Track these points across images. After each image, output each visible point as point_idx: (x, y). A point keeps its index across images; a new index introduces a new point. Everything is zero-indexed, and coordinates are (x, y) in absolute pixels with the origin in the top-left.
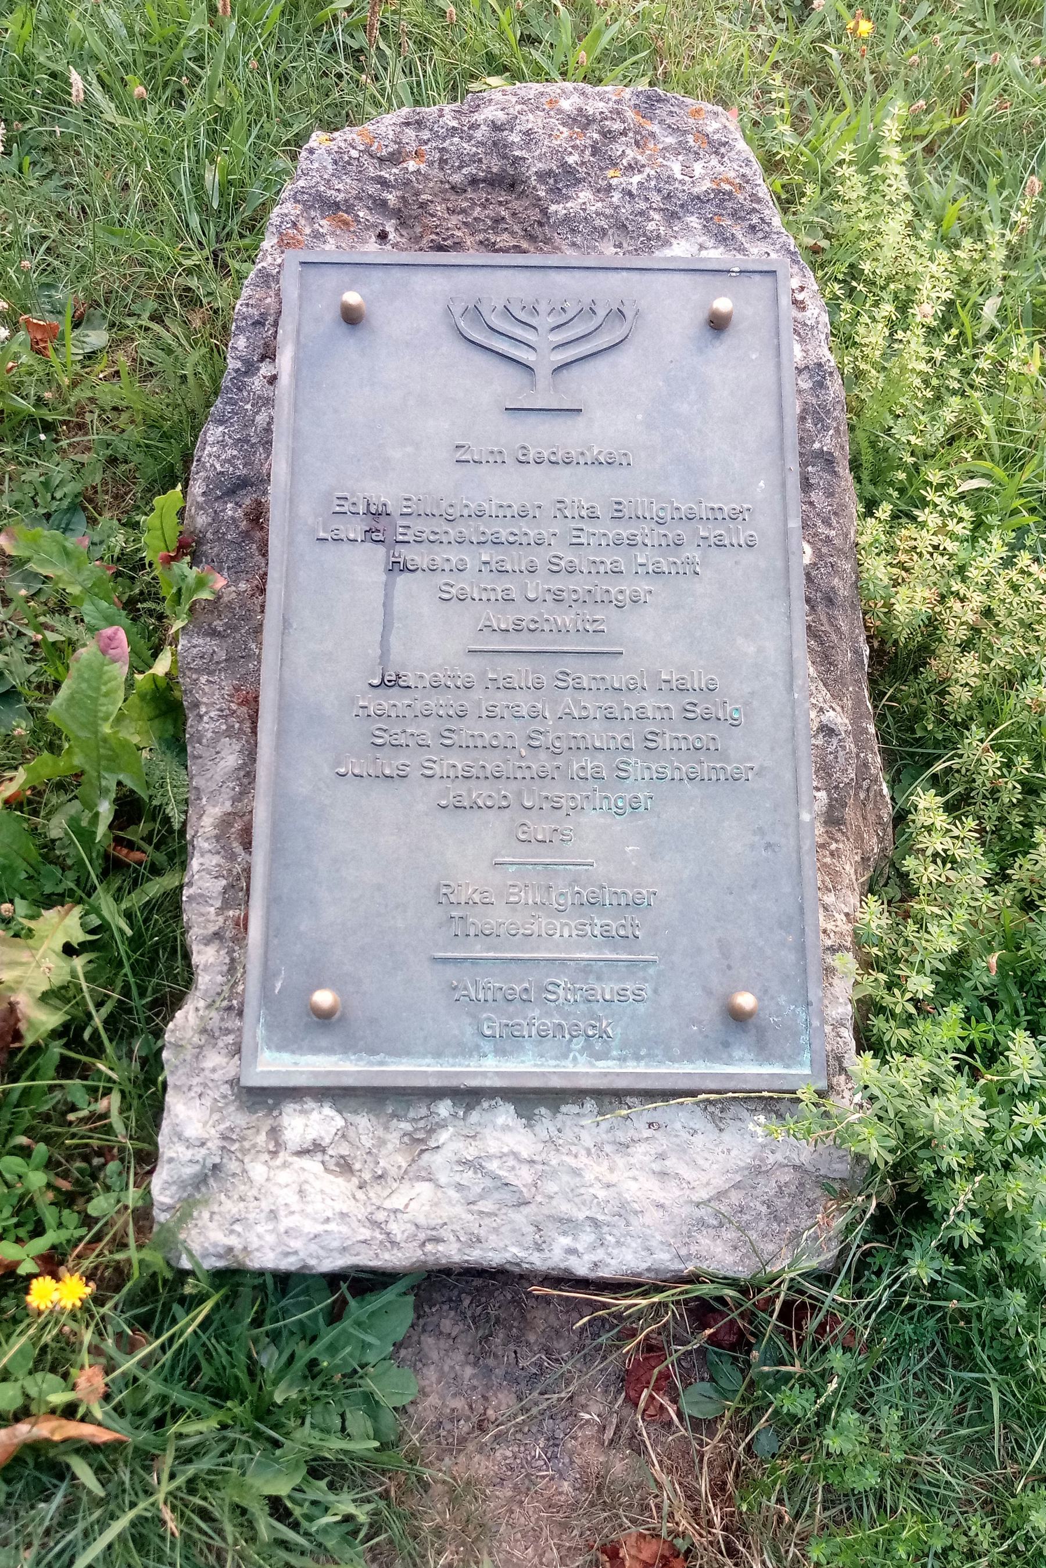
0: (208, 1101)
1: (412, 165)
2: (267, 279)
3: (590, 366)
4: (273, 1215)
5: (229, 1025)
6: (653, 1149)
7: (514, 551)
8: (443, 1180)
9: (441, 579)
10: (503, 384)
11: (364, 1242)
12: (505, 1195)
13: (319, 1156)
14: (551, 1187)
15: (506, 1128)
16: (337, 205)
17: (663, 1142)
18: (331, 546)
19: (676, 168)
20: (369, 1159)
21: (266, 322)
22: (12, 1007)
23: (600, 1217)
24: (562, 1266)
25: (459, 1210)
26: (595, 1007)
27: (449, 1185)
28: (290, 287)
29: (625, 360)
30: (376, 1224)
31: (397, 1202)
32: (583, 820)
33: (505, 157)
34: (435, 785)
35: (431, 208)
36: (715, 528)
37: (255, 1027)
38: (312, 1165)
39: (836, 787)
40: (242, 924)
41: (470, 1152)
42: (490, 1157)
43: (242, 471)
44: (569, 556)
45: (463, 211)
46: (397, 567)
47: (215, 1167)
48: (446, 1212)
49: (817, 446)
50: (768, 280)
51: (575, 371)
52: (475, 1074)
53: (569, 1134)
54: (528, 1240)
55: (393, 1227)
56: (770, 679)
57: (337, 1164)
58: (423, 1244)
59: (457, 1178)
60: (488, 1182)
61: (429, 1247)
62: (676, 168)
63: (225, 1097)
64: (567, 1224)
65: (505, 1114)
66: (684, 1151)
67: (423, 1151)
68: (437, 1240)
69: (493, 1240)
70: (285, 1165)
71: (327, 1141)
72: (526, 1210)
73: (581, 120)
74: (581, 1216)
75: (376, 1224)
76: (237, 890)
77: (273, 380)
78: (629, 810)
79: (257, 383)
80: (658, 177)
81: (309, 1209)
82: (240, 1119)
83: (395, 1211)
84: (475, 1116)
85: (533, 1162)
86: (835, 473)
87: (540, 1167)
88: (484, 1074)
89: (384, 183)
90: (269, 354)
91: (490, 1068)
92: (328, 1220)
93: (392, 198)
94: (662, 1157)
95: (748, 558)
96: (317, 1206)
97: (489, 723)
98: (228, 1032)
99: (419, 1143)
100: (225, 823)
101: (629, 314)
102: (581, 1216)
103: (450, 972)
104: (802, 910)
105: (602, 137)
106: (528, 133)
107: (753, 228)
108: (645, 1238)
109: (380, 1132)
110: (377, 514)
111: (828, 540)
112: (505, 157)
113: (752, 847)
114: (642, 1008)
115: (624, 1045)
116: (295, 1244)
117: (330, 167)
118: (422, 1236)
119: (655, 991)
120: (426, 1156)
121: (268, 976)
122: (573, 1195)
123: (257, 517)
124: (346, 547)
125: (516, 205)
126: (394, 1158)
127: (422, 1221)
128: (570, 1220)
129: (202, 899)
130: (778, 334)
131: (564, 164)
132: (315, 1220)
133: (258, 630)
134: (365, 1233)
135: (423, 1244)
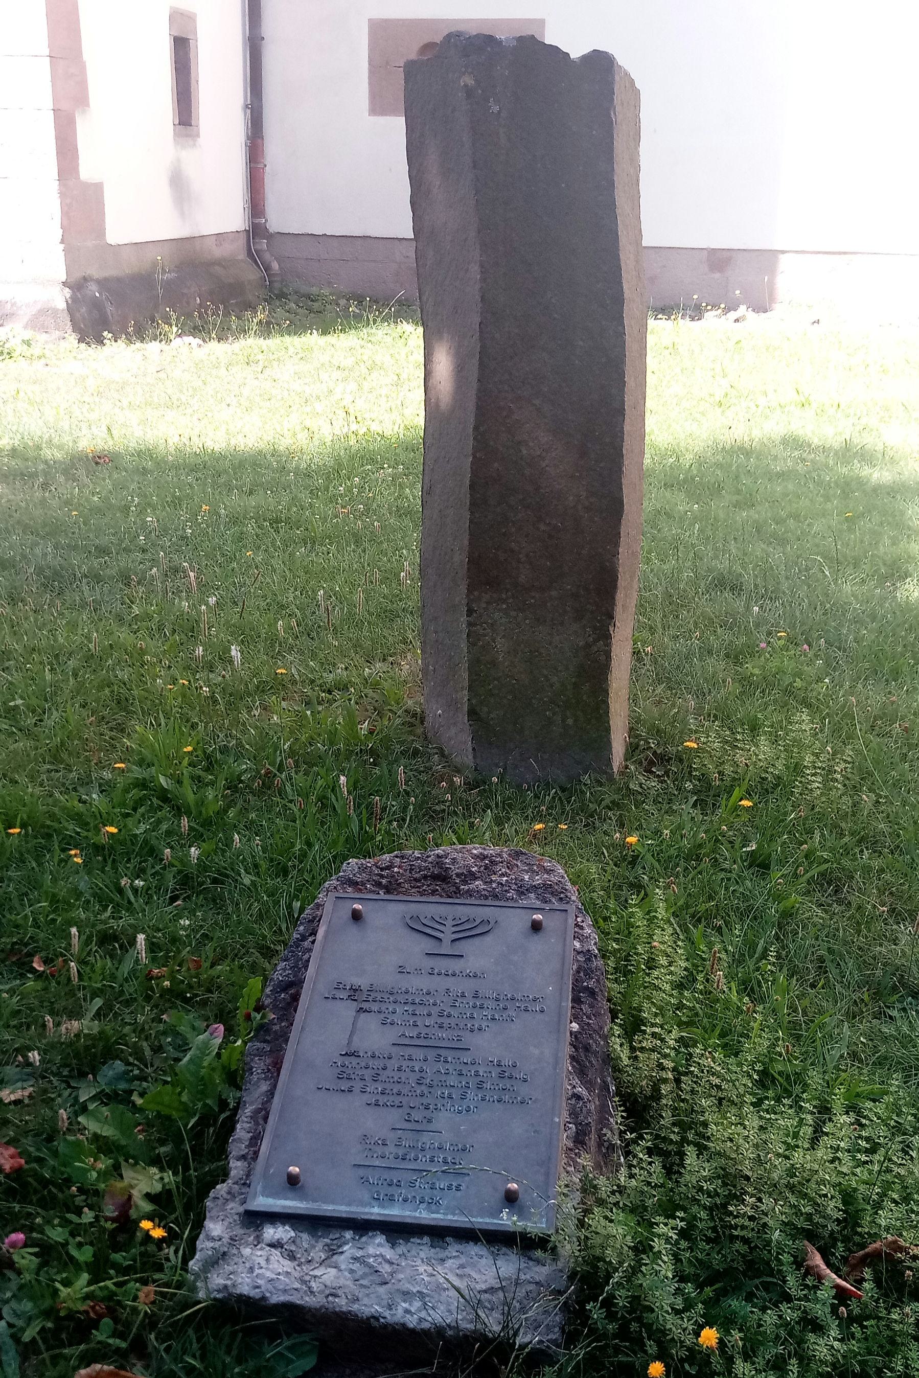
0: (226, 1223)
1: (396, 870)
2: (318, 906)
3: (470, 941)
4: (251, 1269)
5: (243, 1191)
6: (457, 1262)
7: (421, 1007)
8: (343, 1267)
9: (382, 1016)
10: (428, 945)
11: (296, 1290)
12: (374, 1277)
13: (280, 1249)
14: (401, 1276)
15: (379, 1245)
16: (357, 883)
17: (463, 1260)
18: (330, 1002)
19: (527, 878)
20: (305, 1253)
21: (314, 921)
22: (130, 1197)
23: (425, 1291)
24: (402, 1321)
25: (349, 1283)
26: (435, 1192)
27: (346, 1270)
28: (328, 907)
29: (488, 939)
30: (304, 1282)
31: (317, 1273)
32: (440, 1114)
33: (442, 868)
34: (366, 1096)
35: (403, 885)
36: (527, 1005)
37: (258, 1185)
38: (276, 1253)
39: (580, 1124)
40: (256, 1153)
41: (359, 1253)
42: (369, 1256)
43: (292, 978)
44: (448, 1010)
45: (418, 887)
46: (361, 1010)
47: (224, 1254)
48: (342, 1282)
49: (585, 984)
50: (563, 914)
51: (463, 942)
52: (367, 1213)
53: (413, 1252)
54: (385, 1303)
55: (313, 1284)
56: (545, 1065)
57: (288, 1255)
58: (327, 1297)
59: (351, 1266)
60: (367, 1270)
61: (330, 1298)
62: (527, 878)
63: (235, 1221)
64: (407, 1295)
65: (380, 1239)
66: (475, 1266)
67: (334, 1254)
68: (335, 1295)
69: (366, 1301)
70: (261, 1249)
71: (285, 1240)
72: (385, 1287)
73: (483, 857)
74: (415, 1291)
75: (304, 1282)
76: (256, 1140)
77: (313, 942)
78: (464, 1112)
79: (306, 944)
80: (516, 879)
81: (271, 1266)
82: (239, 1231)
83: (315, 1277)
84: (364, 1239)
85: (393, 1263)
86: (596, 999)
87: (395, 1266)
88: (371, 1214)
89: (382, 876)
90: (314, 933)
91: (376, 1212)
92: (279, 1274)
93: (384, 881)
94: (462, 1266)
95: (540, 1016)
96: (274, 1265)
97: (398, 1073)
98: (242, 1194)
99: (332, 1251)
100: (257, 1111)
101: (492, 923)
102: (415, 1291)
103: (361, 1172)
104: (550, 1158)
105: (489, 865)
106: (454, 859)
107: (561, 898)
108: (449, 1304)
109: (313, 1242)
110: (355, 990)
111: (589, 1024)
112: (442, 868)
113: (527, 1131)
114: (459, 1193)
115: (447, 1208)
116: (260, 1282)
117: (356, 870)
118: (327, 1292)
119: (467, 1187)
120: (335, 1257)
121: (267, 1167)
122: (412, 1280)
123: (296, 998)
124: (338, 1002)
125: (444, 886)
126: (318, 1253)
127: (328, 1283)
128: (408, 1293)
129: (240, 1140)
130: (565, 933)
131: (470, 871)
132: (273, 1272)
133: (287, 1041)
134: (297, 1285)
135: (327, 1297)
